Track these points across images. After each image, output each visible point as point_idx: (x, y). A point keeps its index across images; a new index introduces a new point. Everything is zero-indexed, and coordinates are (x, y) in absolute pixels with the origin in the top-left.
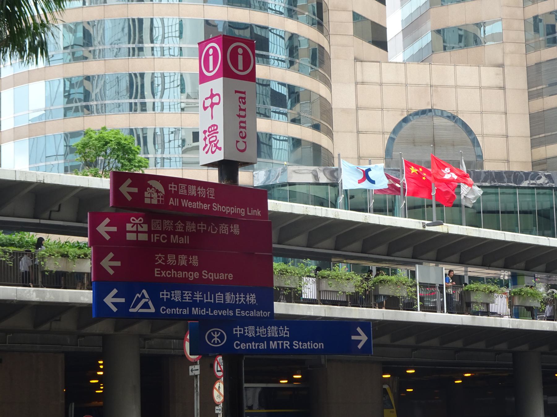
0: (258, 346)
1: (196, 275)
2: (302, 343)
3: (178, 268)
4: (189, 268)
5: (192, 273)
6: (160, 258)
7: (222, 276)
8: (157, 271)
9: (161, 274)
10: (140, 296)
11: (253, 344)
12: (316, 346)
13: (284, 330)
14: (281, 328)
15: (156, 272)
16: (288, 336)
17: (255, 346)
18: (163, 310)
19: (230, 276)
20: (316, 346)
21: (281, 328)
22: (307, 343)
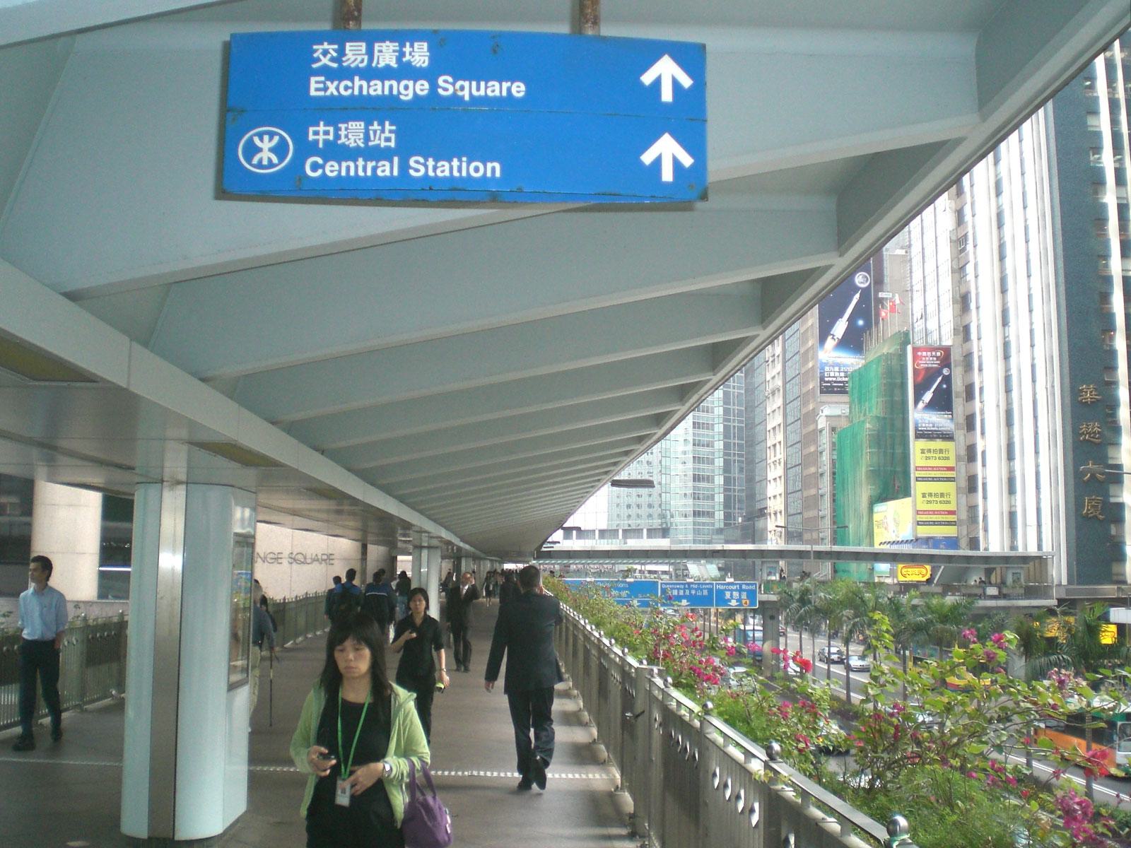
0: (374, 169)
1: (422, 87)
2: (436, 161)
3: (370, 73)
4: (405, 71)
5: (411, 83)
7: (495, 89)
8: (317, 82)
9: (326, 89)
11: (361, 162)
13: (383, 131)
15: (313, 86)
16: (392, 144)
17: (365, 169)
18: (315, 167)
19: (519, 89)
22: (450, 161)
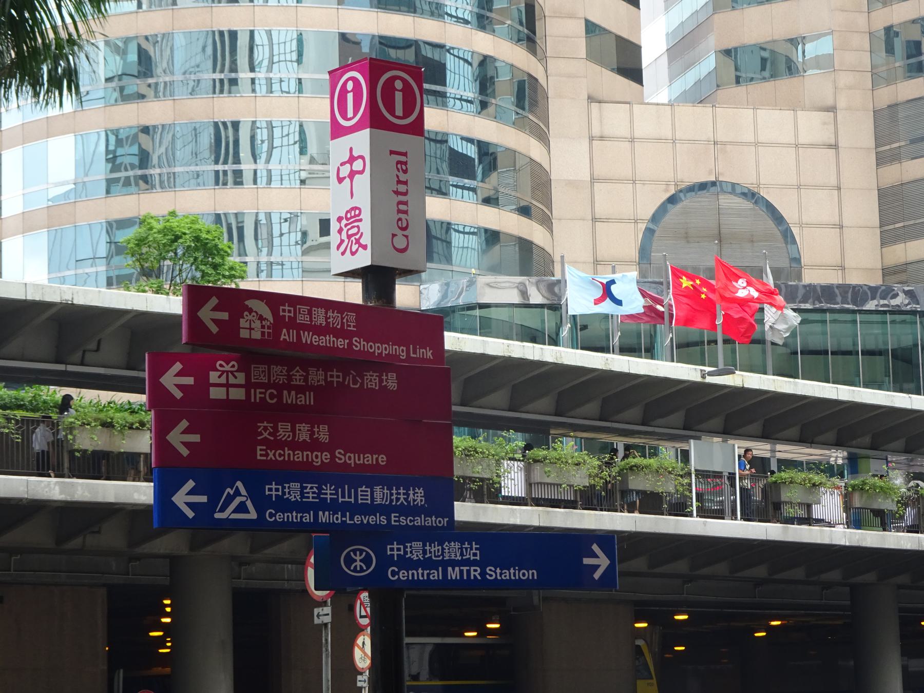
0: (428, 575)
1: (326, 457)
2: (501, 570)
3: (295, 445)
4: (314, 445)
5: (319, 454)
6: (265, 429)
7: (369, 459)
8: (261, 450)
9: (267, 455)
10: (232, 492)
12: (524, 575)
13: (471, 549)
14: (466, 545)
15: (259, 452)
16: (478, 558)
17: (423, 576)
18: (271, 515)
19: (382, 459)
20: (524, 575)
21: (466, 545)
22: (509, 570)
